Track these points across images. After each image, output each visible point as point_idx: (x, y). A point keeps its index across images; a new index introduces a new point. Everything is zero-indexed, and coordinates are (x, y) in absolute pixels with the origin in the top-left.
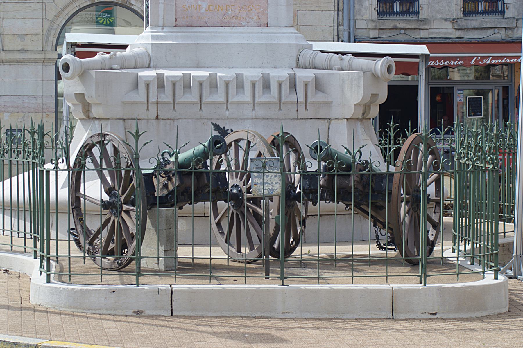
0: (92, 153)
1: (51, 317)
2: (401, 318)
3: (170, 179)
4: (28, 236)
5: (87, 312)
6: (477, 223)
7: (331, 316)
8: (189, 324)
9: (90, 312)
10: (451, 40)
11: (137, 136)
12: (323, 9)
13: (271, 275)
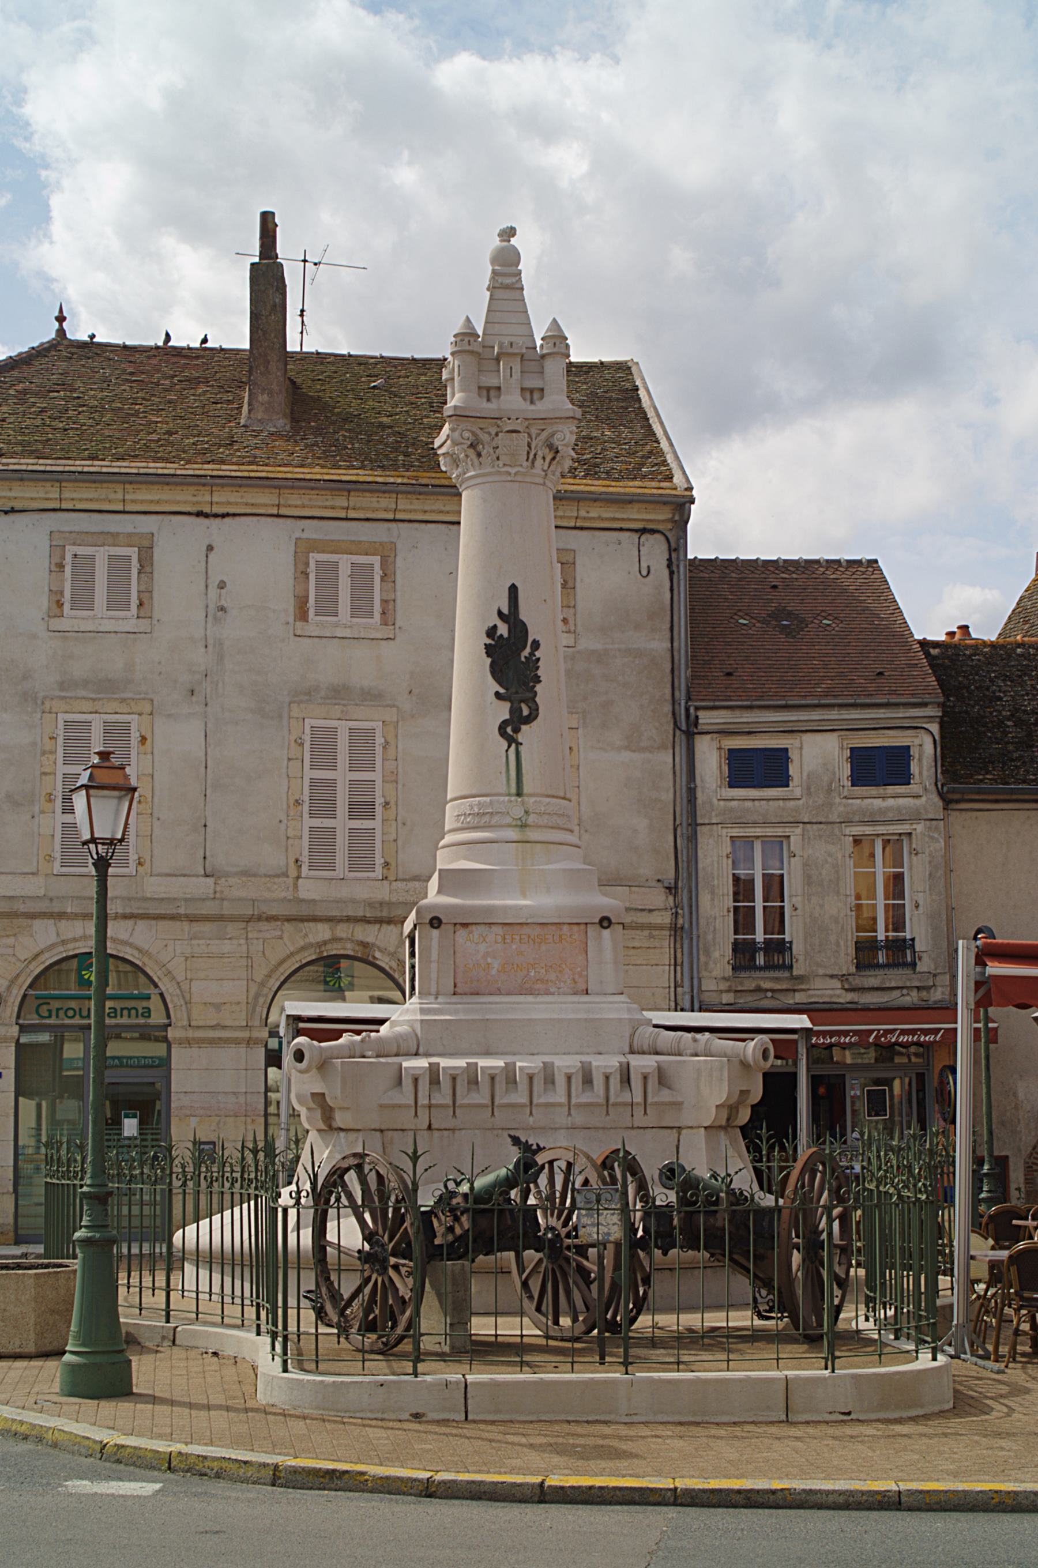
0: (344, 1181)
1: (291, 1422)
2: (800, 1419)
3: (457, 1219)
4: (247, 1302)
5: (342, 1414)
6: (903, 1277)
7: (698, 1419)
8: (493, 1432)
9: (347, 1414)
10: (839, 1006)
11: (415, 1158)
12: (653, 962)
13: (608, 1359)
